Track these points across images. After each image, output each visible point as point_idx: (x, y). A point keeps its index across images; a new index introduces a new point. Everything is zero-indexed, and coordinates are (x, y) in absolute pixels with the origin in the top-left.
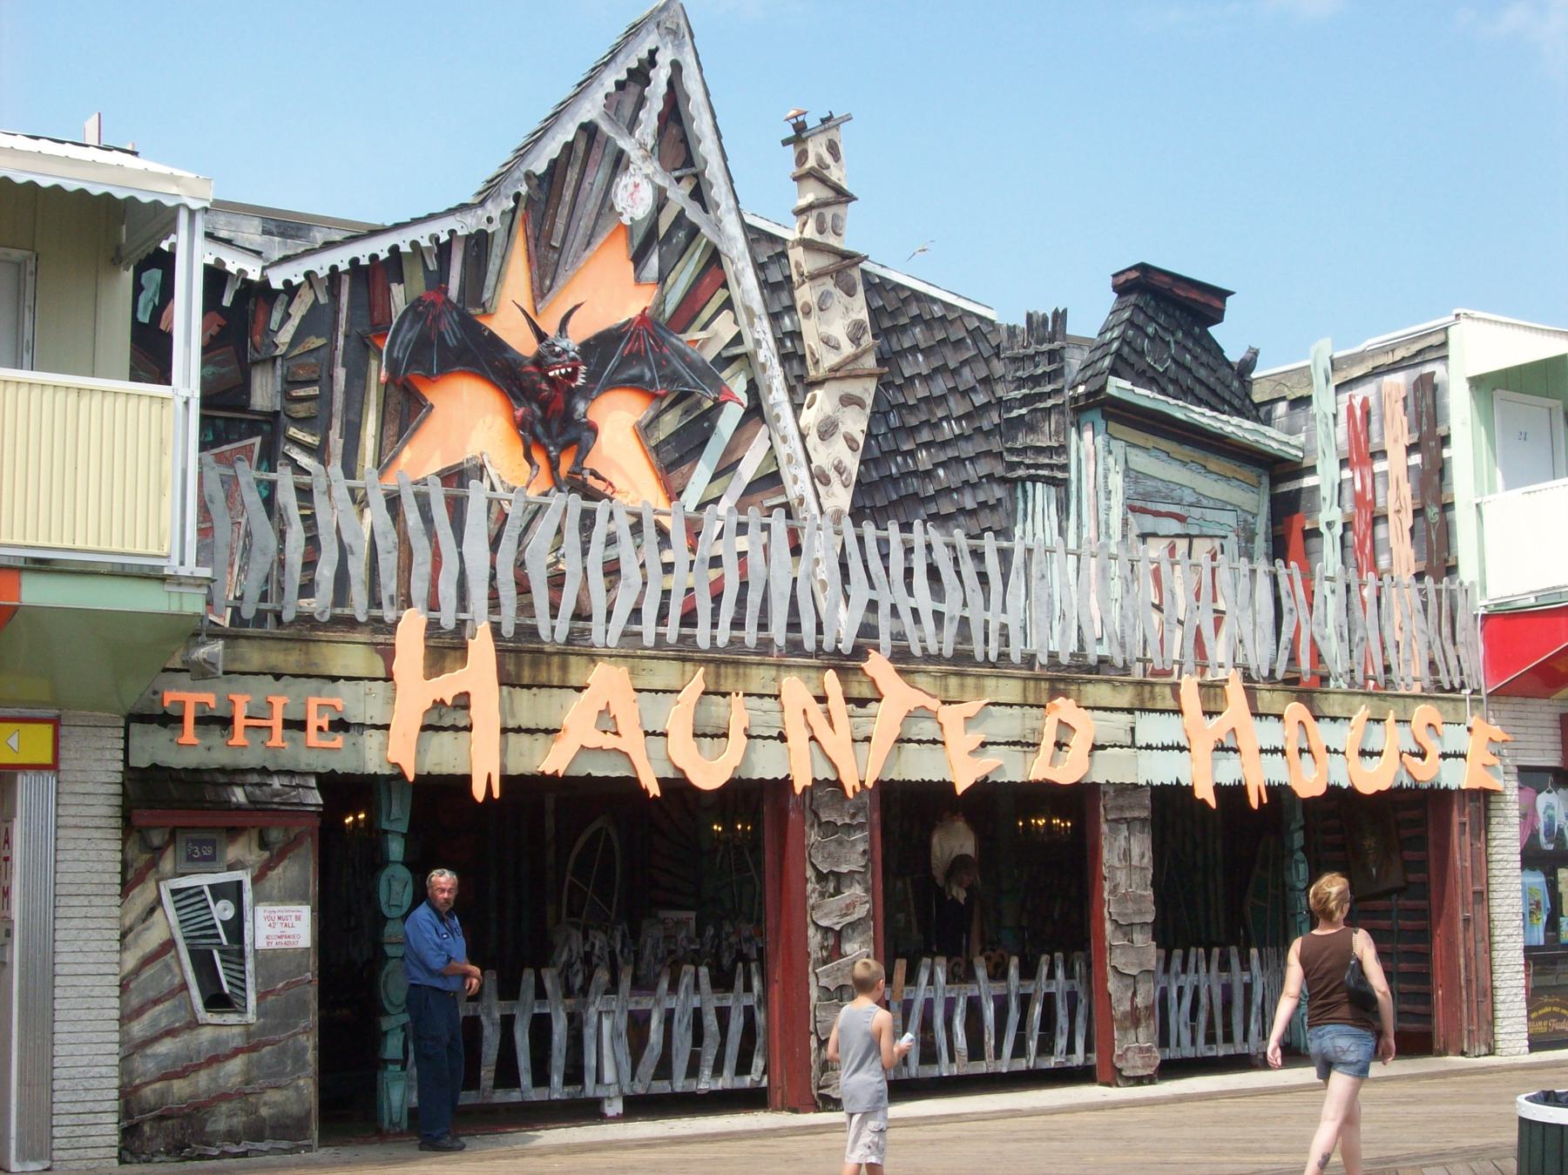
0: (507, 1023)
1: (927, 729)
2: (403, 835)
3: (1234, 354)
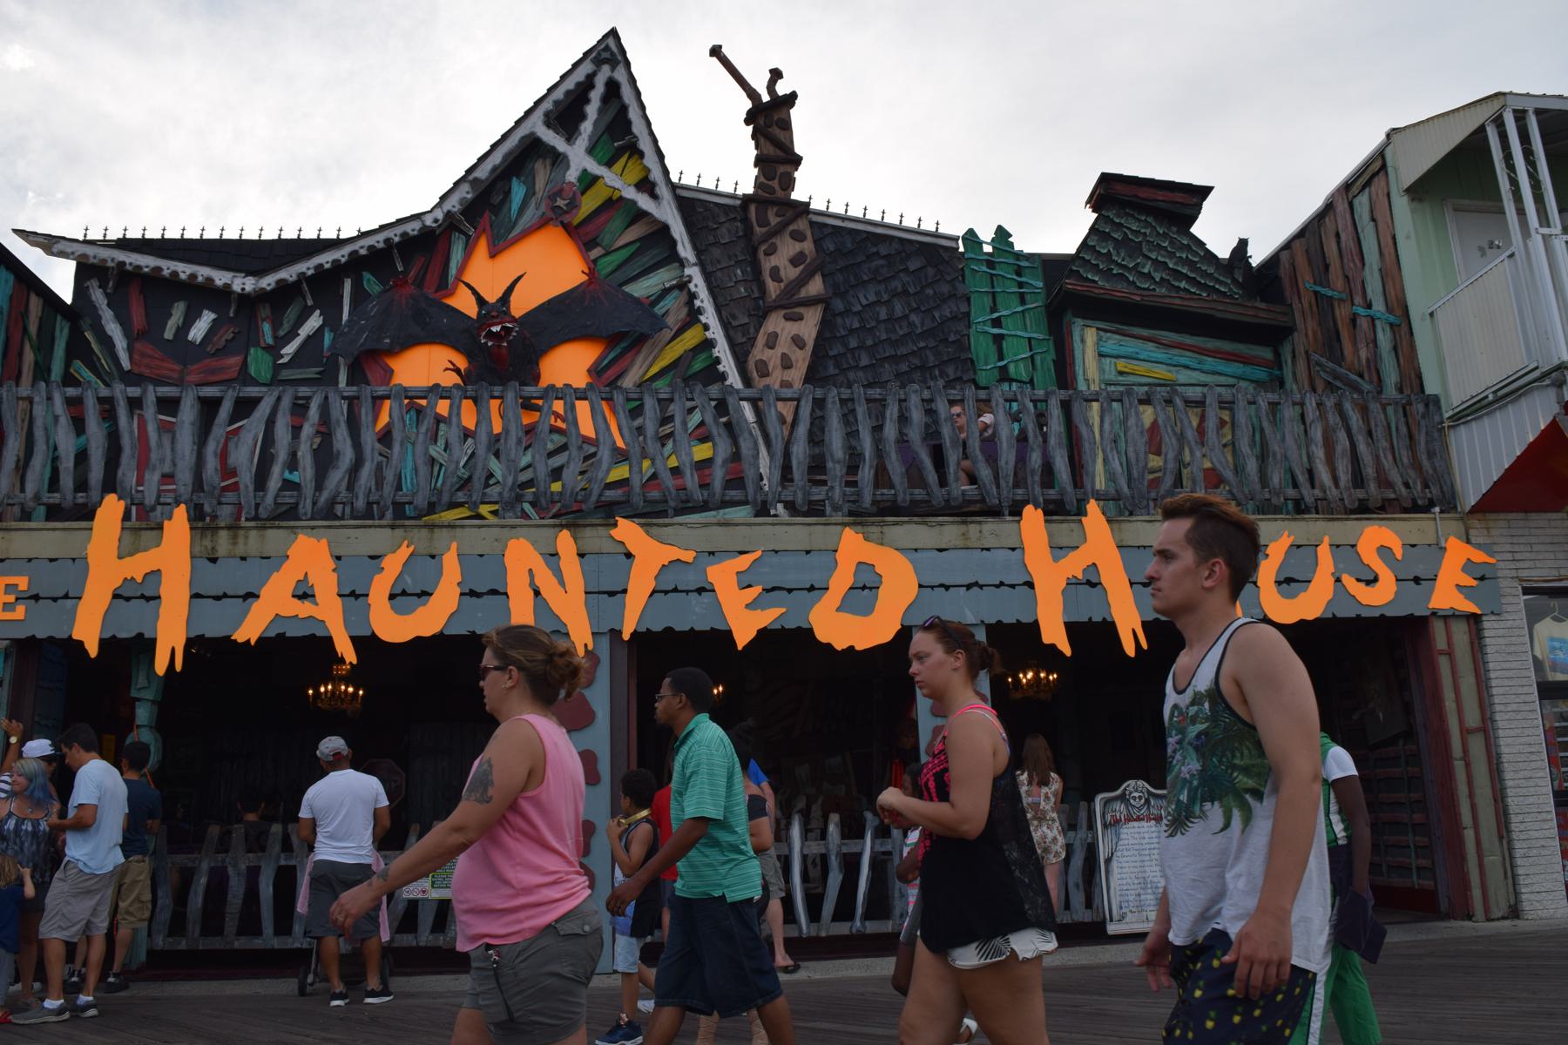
0: (253, 873)
1: (690, 580)
2: (153, 702)
3: (1223, 251)
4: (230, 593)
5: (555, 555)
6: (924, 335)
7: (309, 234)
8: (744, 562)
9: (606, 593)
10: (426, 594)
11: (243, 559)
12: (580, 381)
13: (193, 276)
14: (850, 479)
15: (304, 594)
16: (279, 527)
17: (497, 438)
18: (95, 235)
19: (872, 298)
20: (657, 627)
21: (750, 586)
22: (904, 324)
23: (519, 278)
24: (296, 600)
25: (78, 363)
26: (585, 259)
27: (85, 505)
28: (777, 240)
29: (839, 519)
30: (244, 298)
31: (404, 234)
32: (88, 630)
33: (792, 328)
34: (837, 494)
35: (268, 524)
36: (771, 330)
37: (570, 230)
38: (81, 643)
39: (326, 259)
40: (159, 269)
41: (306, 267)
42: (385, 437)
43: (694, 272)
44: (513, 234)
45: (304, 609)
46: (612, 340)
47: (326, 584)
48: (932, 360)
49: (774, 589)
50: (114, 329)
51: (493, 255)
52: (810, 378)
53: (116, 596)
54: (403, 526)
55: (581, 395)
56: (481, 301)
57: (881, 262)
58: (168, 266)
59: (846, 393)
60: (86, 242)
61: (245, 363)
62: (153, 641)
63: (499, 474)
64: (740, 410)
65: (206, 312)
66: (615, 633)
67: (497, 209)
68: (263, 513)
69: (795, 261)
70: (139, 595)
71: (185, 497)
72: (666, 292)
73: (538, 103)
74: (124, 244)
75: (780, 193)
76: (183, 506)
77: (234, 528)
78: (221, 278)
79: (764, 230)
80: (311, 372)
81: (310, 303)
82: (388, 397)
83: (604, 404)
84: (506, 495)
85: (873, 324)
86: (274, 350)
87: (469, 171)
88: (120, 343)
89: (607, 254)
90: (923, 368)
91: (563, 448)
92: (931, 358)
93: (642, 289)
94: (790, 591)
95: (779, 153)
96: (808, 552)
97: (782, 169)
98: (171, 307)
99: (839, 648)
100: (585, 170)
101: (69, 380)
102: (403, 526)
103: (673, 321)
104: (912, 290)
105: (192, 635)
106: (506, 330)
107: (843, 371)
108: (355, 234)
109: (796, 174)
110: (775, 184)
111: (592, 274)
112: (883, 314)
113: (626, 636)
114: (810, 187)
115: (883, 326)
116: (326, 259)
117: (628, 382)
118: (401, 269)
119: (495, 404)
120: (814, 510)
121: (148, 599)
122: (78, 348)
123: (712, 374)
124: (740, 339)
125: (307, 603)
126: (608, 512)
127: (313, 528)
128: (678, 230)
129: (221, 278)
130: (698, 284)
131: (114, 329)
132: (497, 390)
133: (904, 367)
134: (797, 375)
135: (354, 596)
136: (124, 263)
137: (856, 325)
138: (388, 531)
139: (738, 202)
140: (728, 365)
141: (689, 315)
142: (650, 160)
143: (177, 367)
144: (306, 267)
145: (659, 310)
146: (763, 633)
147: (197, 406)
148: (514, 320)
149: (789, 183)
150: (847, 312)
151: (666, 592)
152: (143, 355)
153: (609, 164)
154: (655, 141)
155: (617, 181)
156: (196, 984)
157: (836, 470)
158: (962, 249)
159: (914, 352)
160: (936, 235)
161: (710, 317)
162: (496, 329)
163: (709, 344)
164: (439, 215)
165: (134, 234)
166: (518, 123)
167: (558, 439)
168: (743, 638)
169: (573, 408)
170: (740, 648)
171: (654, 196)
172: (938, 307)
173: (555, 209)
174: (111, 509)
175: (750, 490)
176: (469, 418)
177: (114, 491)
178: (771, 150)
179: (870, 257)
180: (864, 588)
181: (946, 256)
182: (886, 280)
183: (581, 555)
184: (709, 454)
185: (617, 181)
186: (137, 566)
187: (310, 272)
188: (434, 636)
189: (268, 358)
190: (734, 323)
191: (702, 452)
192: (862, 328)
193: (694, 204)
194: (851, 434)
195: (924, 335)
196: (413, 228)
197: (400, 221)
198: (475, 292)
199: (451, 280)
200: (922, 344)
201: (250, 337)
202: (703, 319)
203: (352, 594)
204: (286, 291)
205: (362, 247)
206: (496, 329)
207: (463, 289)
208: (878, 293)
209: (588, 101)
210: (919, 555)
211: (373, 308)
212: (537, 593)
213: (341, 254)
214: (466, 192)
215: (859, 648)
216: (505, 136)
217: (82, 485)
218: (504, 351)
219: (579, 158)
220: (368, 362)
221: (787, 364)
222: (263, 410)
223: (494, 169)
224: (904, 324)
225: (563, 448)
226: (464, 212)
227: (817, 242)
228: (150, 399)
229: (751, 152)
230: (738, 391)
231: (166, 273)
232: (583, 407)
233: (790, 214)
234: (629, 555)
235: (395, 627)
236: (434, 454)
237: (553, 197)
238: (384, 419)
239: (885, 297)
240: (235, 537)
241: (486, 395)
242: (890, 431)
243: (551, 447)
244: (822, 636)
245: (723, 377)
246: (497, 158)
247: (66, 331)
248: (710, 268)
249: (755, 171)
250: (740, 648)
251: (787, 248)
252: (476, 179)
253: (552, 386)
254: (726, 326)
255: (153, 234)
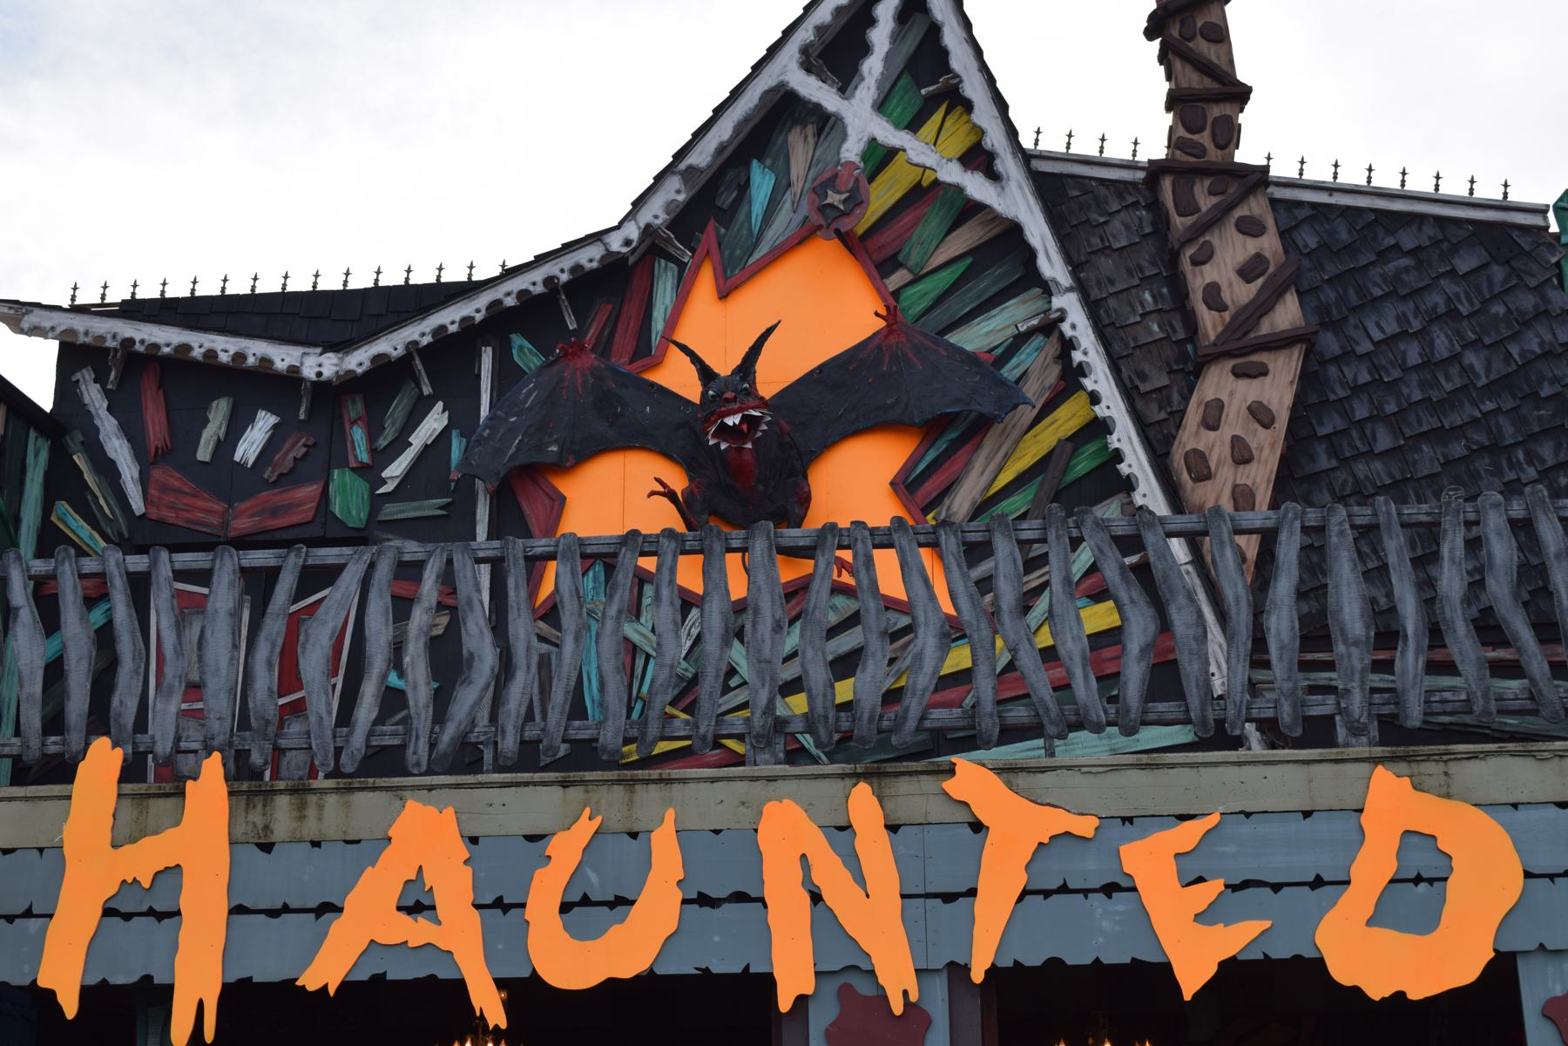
1: (1090, 870)
4: (293, 904)
5: (845, 828)
6: (1492, 389)
7: (423, 276)
8: (1188, 835)
9: (940, 897)
10: (622, 902)
11: (316, 844)
12: (881, 510)
13: (240, 356)
14: (1382, 656)
15: (417, 906)
16: (375, 789)
17: (740, 607)
18: (89, 296)
19: (1392, 328)
20: (1034, 959)
21: (1200, 880)
22: (1454, 370)
23: (769, 331)
24: (402, 916)
25: (63, 507)
26: (880, 291)
27: (60, 755)
28: (1213, 238)
29: (1364, 750)
30: (321, 388)
31: (577, 268)
32: (63, 974)
33: (1250, 391)
34: (1357, 702)
35: (356, 782)
36: (1210, 397)
37: (853, 244)
38: (51, 994)
39: (450, 317)
40: (186, 348)
41: (419, 332)
42: (551, 613)
43: (1069, 304)
44: (756, 256)
45: (417, 931)
46: (931, 429)
47: (454, 887)
48: (1509, 432)
49: (1246, 884)
50: (118, 449)
51: (724, 295)
52: (1291, 480)
53: (108, 912)
54: (583, 782)
55: (883, 539)
56: (706, 374)
57: (1405, 262)
58: (200, 343)
59: (1363, 515)
60: (76, 309)
61: (325, 496)
62: (167, 991)
63: (744, 669)
64: (1166, 553)
65: (261, 414)
66: (957, 971)
67: (727, 216)
68: (348, 765)
69: (1247, 272)
70: (146, 909)
71: (220, 740)
72: (1020, 339)
73: (788, 32)
74: (134, 309)
75: (1214, 155)
76: (217, 756)
77: (299, 791)
78: (283, 357)
79: (1189, 220)
80: (430, 507)
81: (427, 390)
82: (552, 556)
83: (925, 555)
84: (757, 722)
85: (1396, 373)
86: (370, 472)
87: (680, 155)
88: (129, 471)
89: (917, 280)
90: (1495, 449)
91: (853, 620)
92: (1508, 429)
93: (977, 337)
94: (1276, 887)
95: (1208, 83)
96: (1307, 814)
97: (1215, 111)
98: (207, 408)
99: (1377, 998)
100: (873, 140)
101: (50, 540)
102: (583, 782)
103: (1035, 390)
104: (1464, 309)
105: (232, 979)
106: (752, 422)
107: (1345, 462)
108: (497, 272)
109: (1242, 118)
110: (1205, 138)
111: (891, 316)
112: (1413, 355)
113: (978, 976)
114: (1269, 138)
115: (1414, 378)
116: (450, 317)
117: (961, 502)
118: (585, 308)
119: (733, 561)
120: (1318, 733)
121: (161, 916)
122: (62, 482)
123: (1110, 480)
124: (1155, 414)
125: (422, 921)
126: (937, 747)
127: (431, 788)
128: (1038, 232)
129: (283, 357)
130: (1078, 324)
131: (118, 449)
132: (737, 537)
133: (1458, 449)
134: (1261, 475)
135: (501, 907)
136: (131, 341)
137: (1364, 377)
138: (557, 790)
139: (1141, 175)
140: (1136, 462)
141: (1062, 377)
142: (984, 114)
143: (219, 507)
144: (419, 332)
145: (1010, 372)
146: (1228, 967)
147: (239, 584)
148: (763, 403)
149: (1230, 135)
150: (1347, 356)
151: (1047, 894)
152: (165, 489)
153: (914, 126)
154: (991, 80)
155: (929, 154)
156: (755, 100)
157: (1352, 655)
158: (1554, 228)
159: (1474, 422)
160: (1504, 206)
161: (1100, 379)
162: (731, 421)
163: (1101, 427)
164: (632, 231)
165: (148, 292)
166: (758, 68)
167: (845, 605)
168: (1192, 977)
169: (869, 563)
170: (1188, 996)
171: (993, 176)
172: (1514, 337)
173: (824, 209)
174: (102, 762)
175: (1194, 701)
176: (689, 573)
177: (107, 733)
178: (1193, 80)
179: (1382, 256)
180: (1418, 880)
181: (1525, 243)
182: (1416, 293)
183: (892, 828)
184: (1113, 620)
185: (929, 154)
186: (143, 859)
187: (426, 341)
188: (638, 978)
189: (361, 486)
190: (1144, 387)
191: (1099, 617)
192: (1377, 382)
193: (1066, 187)
194: (1377, 574)
195: (1492, 389)
196: (589, 257)
197: (568, 247)
198: (695, 359)
199: (655, 339)
200: (1489, 406)
201: (333, 453)
202: (1088, 383)
203: (499, 904)
204: (387, 374)
205: (508, 294)
206: (731, 421)
207: (675, 355)
208: (1402, 319)
209: (872, 22)
210: (1522, 814)
211: (528, 394)
212: (816, 898)
213: (474, 308)
214: (676, 191)
215: (1414, 995)
216: (736, 93)
217: (54, 723)
218: (747, 457)
219: (861, 118)
220: (523, 491)
221: (1241, 454)
222: (349, 581)
223: (721, 149)
224: (1454, 370)
225: (853, 620)
226: (671, 226)
227: (1285, 235)
228: (164, 571)
229: (1160, 87)
230: (1162, 521)
231: (197, 353)
232: (886, 563)
233: (1233, 189)
234: (977, 827)
235: (572, 963)
236: (635, 638)
237: (820, 190)
238: (547, 588)
239: (1416, 325)
240: (302, 807)
241: (718, 547)
242: (1451, 580)
243: (833, 619)
244: (1342, 972)
245: (1128, 485)
246: (724, 131)
247: (44, 456)
248: (1096, 294)
249: (1168, 119)
250: (1188, 996)
251: (1232, 249)
252: (690, 168)
253: (832, 527)
254: (1129, 393)
255: (178, 290)
